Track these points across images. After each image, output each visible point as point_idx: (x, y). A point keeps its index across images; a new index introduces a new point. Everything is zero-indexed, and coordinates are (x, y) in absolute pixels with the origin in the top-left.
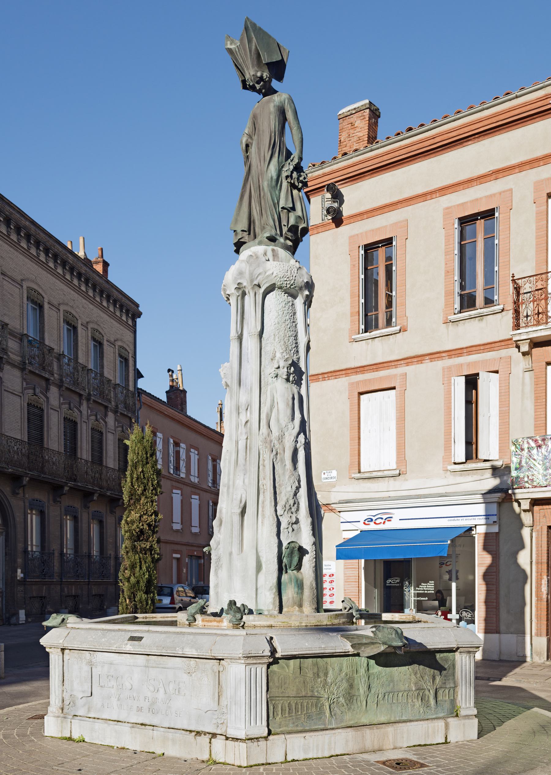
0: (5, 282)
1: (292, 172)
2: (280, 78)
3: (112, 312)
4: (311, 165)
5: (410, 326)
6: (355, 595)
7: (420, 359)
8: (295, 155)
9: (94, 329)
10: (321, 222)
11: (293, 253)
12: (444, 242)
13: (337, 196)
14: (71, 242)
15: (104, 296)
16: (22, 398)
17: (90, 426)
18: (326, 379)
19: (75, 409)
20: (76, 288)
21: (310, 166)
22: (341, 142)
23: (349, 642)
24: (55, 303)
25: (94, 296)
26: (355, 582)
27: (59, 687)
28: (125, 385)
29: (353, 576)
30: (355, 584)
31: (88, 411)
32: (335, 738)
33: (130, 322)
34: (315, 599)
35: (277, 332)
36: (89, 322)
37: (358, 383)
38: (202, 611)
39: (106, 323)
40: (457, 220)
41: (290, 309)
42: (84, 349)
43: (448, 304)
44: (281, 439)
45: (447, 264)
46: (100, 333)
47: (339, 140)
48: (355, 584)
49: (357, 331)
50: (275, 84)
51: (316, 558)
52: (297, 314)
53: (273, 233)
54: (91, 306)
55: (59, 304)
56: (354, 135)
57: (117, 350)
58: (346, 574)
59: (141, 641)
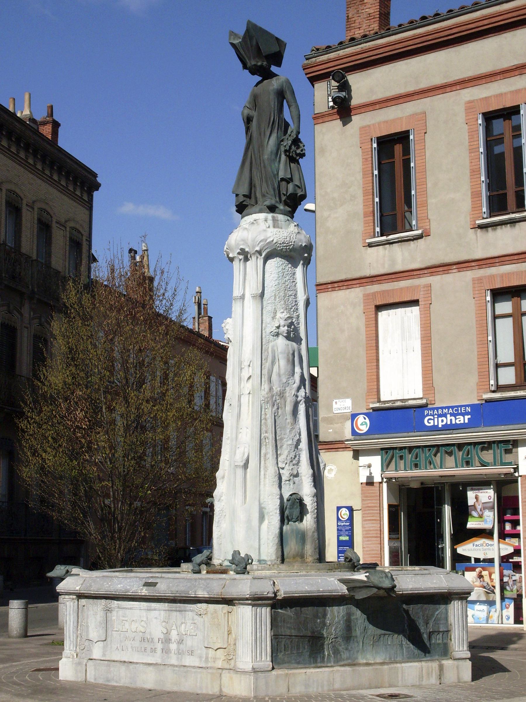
1: (290, 147)
2: (279, 64)
3: (63, 186)
4: (315, 49)
5: (434, 228)
6: (376, 554)
7: (446, 268)
8: (292, 127)
9: (41, 209)
10: (327, 110)
11: (292, 217)
12: (467, 138)
13: (344, 86)
14: (14, 99)
15: (55, 168)
17: (32, 334)
18: (337, 289)
19: (15, 312)
20: (23, 161)
21: (313, 50)
22: (349, 17)
23: (345, 586)
24: (63, 220)
25: (43, 169)
26: (376, 537)
27: (73, 632)
29: (373, 530)
30: (377, 540)
31: (30, 312)
32: (334, 675)
33: (85, 197)
34: (317, 550)
35: (277, 292)
36: (35, 201)
37: (374, 294)
38: (208, 561)
40: (481, 115)
41: (290, 270)
43: (476, 207)
44: (282, 395)
45: (472, 162)
46: (48, 213)
47: (347, 15)
48: (377, 540)
49: (372, 234)
50: (274, 69)
51: (317, 509)
52: (296, 274)
53: (273, 202)
54: (39, 181)
56: (363, 11)
57: (68, 233)
58: (365, 528)
59: (155, 586)
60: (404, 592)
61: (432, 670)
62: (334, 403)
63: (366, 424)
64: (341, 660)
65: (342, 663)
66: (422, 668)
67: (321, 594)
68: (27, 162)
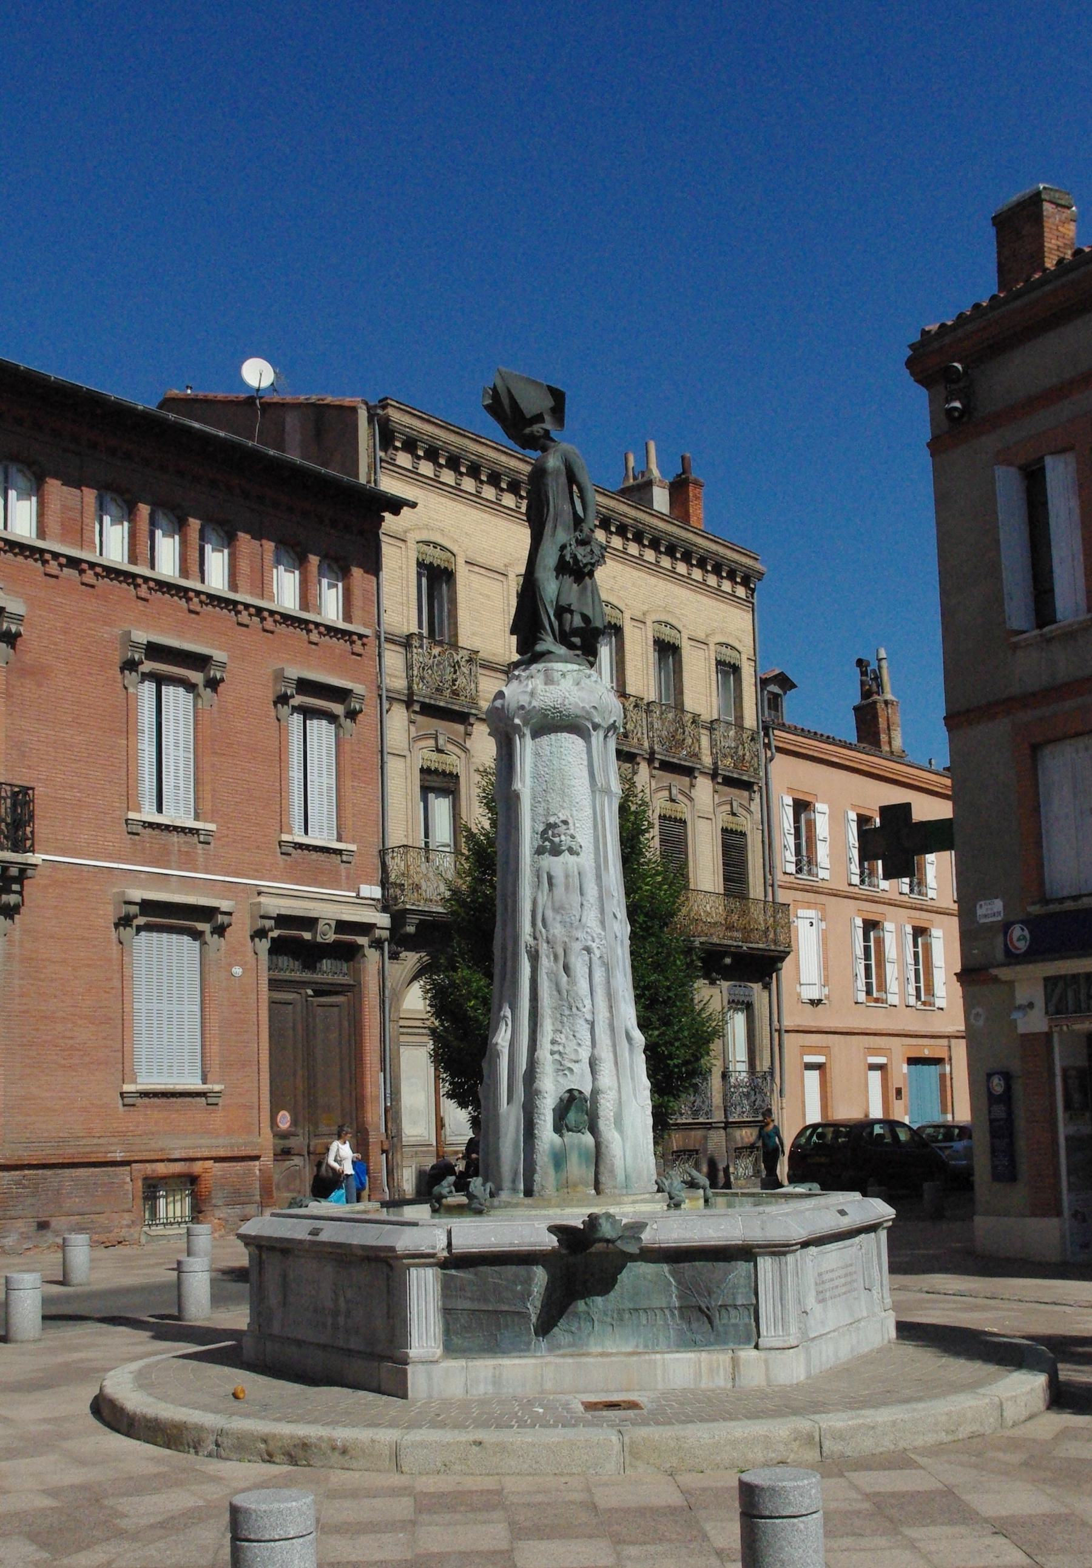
0: (473, 577)
16: (714, 820)
24: (701, 636)
28: (736, 718)
39: (686, 605)
42: (639, 665)
55: (405, 532)
60: (662, 1245)
61: (719, 1365)
62: (978, 907)
63: (1024, 938)
64: (559, 1347)
65: (561, 1352)
66: (700, 1362)
67: (517, 1248)
68: (627, 554)
